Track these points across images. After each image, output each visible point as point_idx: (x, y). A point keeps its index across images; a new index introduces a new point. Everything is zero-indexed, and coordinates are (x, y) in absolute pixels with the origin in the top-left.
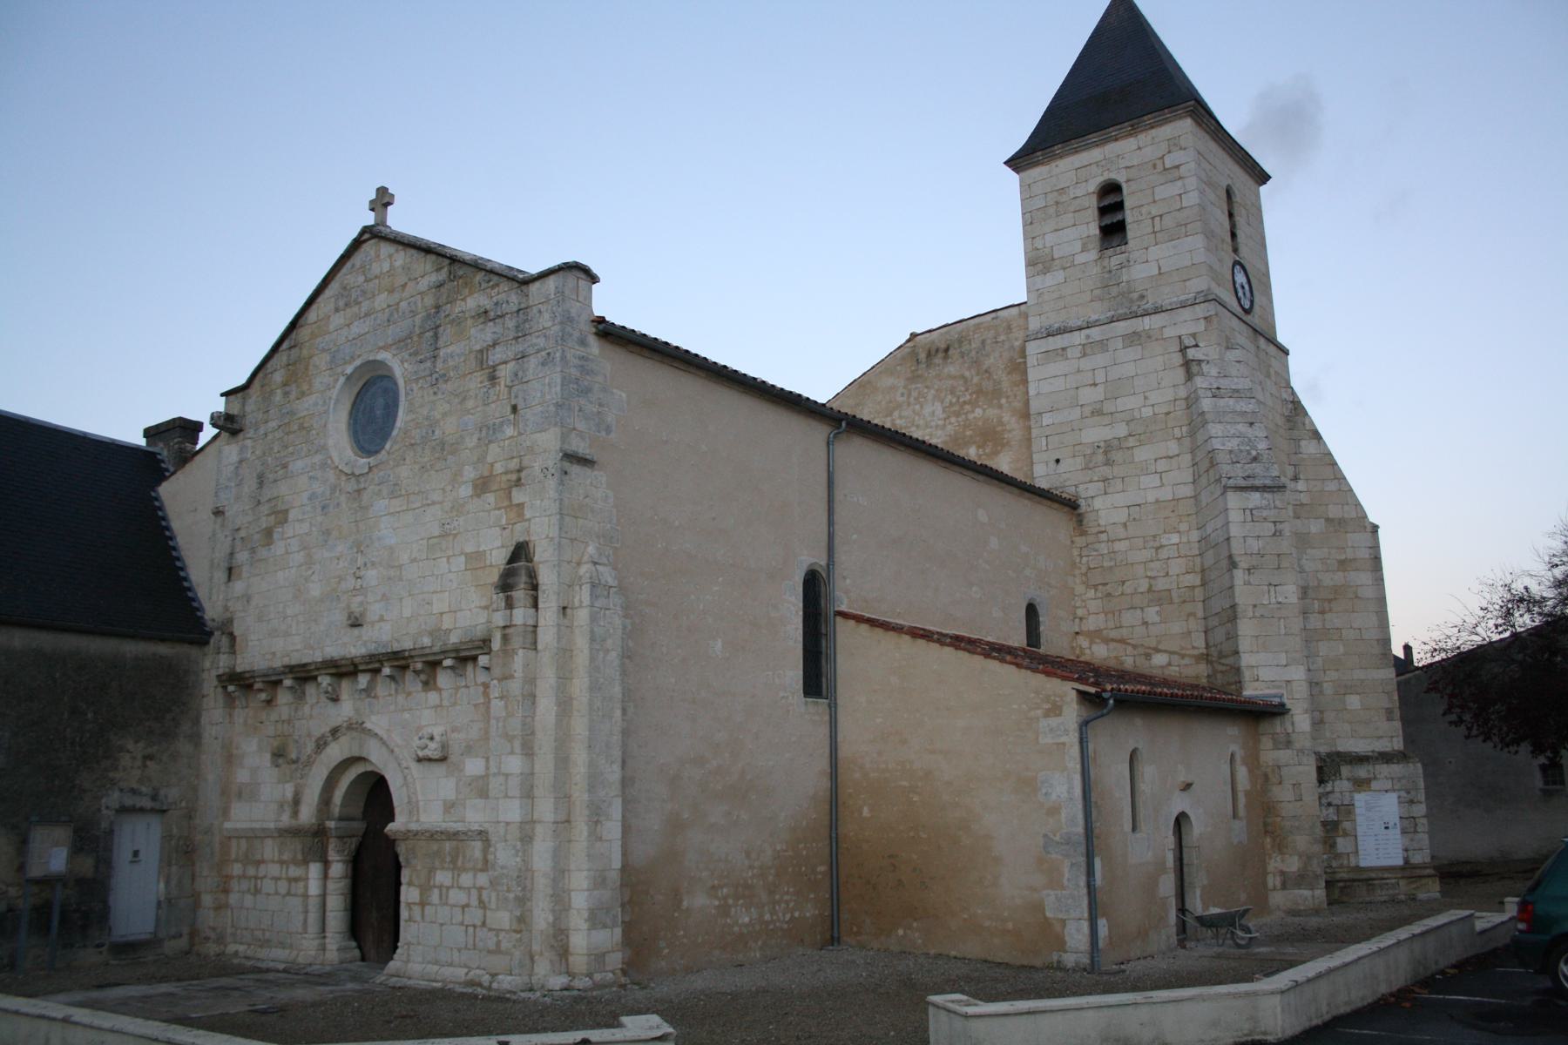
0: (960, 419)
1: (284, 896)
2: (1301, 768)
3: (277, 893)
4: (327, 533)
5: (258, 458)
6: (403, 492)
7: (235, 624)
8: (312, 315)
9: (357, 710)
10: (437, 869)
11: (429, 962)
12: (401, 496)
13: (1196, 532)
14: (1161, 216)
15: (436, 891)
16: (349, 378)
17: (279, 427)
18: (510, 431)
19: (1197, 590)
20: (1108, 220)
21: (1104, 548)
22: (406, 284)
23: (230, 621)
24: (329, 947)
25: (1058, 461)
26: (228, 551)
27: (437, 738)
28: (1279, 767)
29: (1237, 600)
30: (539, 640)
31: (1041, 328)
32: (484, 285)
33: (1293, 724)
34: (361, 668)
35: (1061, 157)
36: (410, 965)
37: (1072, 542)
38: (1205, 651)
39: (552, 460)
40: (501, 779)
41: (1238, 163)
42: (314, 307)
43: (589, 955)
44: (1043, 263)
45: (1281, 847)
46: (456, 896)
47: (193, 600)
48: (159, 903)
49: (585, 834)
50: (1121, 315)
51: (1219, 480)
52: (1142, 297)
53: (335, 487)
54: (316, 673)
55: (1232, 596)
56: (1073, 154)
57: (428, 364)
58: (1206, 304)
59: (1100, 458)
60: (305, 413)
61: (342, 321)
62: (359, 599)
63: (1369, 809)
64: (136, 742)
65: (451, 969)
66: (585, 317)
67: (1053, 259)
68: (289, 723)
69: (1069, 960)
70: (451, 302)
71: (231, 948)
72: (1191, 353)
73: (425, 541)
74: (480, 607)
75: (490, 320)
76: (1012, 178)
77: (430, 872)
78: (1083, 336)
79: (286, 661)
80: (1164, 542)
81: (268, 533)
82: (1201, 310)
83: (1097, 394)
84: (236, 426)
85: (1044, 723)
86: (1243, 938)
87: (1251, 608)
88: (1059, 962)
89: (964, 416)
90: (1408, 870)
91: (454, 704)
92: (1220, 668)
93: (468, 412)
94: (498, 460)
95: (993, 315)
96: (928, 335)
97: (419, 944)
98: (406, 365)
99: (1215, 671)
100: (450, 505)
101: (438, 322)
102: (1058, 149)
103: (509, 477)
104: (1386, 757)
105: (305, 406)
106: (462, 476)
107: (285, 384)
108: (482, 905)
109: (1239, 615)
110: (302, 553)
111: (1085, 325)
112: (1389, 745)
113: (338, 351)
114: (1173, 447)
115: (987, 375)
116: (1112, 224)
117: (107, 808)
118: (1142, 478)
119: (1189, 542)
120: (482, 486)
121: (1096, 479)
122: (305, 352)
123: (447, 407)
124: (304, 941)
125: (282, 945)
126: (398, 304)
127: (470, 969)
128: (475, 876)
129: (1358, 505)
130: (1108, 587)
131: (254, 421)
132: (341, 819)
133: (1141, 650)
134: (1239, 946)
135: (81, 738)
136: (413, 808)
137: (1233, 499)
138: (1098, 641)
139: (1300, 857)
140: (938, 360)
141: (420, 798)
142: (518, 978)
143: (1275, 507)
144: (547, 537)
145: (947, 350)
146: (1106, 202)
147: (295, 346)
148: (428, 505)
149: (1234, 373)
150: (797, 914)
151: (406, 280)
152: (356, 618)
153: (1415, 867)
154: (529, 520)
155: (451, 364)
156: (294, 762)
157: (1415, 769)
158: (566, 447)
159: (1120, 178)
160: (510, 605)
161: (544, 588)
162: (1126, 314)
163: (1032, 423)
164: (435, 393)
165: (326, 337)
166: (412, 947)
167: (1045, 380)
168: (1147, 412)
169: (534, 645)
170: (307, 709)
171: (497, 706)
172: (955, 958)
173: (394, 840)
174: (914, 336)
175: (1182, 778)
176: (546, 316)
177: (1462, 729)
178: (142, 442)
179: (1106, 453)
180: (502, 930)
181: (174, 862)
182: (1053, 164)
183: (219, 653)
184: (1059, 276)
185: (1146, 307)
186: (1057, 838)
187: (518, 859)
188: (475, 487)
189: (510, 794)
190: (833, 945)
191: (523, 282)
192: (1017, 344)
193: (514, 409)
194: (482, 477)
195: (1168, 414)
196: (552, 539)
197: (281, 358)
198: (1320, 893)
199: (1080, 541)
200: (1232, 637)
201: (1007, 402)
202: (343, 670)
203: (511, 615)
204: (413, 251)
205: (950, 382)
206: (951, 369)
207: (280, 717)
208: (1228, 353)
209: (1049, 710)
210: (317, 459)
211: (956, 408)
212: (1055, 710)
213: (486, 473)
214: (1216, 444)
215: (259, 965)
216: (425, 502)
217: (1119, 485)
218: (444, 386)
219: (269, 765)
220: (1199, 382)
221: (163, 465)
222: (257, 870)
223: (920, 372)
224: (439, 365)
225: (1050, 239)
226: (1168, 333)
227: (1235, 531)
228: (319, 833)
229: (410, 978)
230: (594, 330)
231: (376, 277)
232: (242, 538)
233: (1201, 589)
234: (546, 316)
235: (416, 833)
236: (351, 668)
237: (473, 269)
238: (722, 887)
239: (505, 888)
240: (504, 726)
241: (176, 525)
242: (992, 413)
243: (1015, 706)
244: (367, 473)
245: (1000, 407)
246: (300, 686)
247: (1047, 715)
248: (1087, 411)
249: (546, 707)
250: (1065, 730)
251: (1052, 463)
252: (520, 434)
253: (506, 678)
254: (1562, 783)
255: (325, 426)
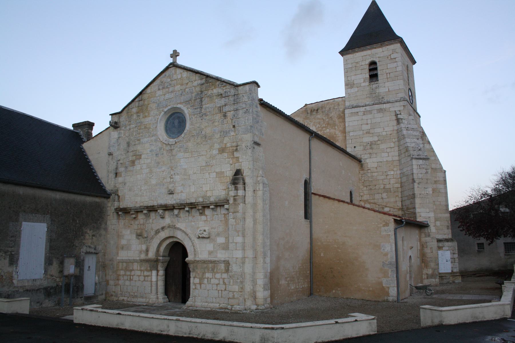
0: (322, 132)
1: (142, 282)
2: (433, 243)
3: (139, 280)
4: (158, 163)
5: (127, 137)
6: (190, 151)
7: (119, 191)
8: (148, 90)
9: (172, 222)
10: (206, 272)
11: (203, 302)
12: (189, 152)
13: (399, 171)
14: (389, 73)
15: (206, 280)
16: (165, 112)
17: (136, 127)
18: (232, 133)
19: (399, 189)
20: (372, 73)
21: (369, 175)
22: (188, 83)
23: (117, 190)
24: (159, 298)
25: (355, 147)
26: (115, 167)
27: (207, 231)
28: (426, 243)
29: (415, 192)
30: (246, 200)
31: (350, 105)
32: (220, 86)
33: (430, 230)
34: (176, 208)
35: (357, 52)
36: (196, 303)
37: (359, 172)
38: (401, 207)
39: (250, 144)
40: (234, 244)
41: (409, 58)
42: (149, 88)
43: (263, 299)
44: (351, 85)
45: (427, 266)
46: (213, 281)
47: (100, 183)
48: (96, 284)
49: (262, 261)
50: (376, 103)
51: (410, 156)
52: (383, 98)
53: (161, 148)
54: (157, 209)
55: (414, 191)
56: (361, 51)
57: (199, 110)
58: (404, 101)
59: (369, 147)
60: (147, 123)
61: (161, 93)
62: (172, 185)
63: (442, 256)
64: (90, 230)
65: (213, 304)
66: (257, 99)
67: (354, 84)
68: (143, 225)
69: (390, 299)
70: (207, 90)
71: (121, 298)
72: (399, 116)
73: (199, 167)
74: (222, 189)
75: (223, 97)
76: (341, 58)
77: (203, 273)
78: (364, 109)
79: (142, 204)
80: (389, 174)
81: (133, 163)
82: (402, 103)
83: (368, 127)
84: (118, 126)
85: (383, 228)
86: (429, 293)
87: (419, 195)
88: (387, 300)
89: (323, 131)
90: (452, 274)
91: (212, 220)
92: (407, 212)
93: (216, 126)
94: (228, 142)
95: (333, 100)
96: (311, 105)
97: (199, 296)
98: (189, 109)
99: (405, 214)
100: (209, 156)
101: (202, 97)
102: (356, 50)
103: (233, 148)
104: (447, 240)
105: (147, 121)
106: (214, 147)
107: (137, 113)
108: (224, 283)
109: (416, 197)
110: (148, 169)
111: (365, 105)
112: (448, 236)
113: (160, 103)
114: (392, 145)
115: (331, 119)
116: (373, 74)
117: (83, 252)
118: (382, 154)
119: (397, 174)
120: (222, 150)
121: (367, 153)
122: (146, 103)
123: (207, 124)
124: (151, 296)
125: (142, 297)
126: (185, 89)
127: (220, 304)
128: (221, 275)
129: (440, 164)
130: (371, 186)
131: (124, 124)
132: (163, 256)
133: (381, 206)
134: (428, 295)
135: (75, 229)
136: (195, 253)
137: (414, 162)
138: (367, 203)
139: (432, 269)
140: (314, 113)
141: (198, 250)
142: (242, 306)
143: (426, 165)
144: (248, 168)
145: (317, 110)
146: (371, 67)
147: (141, 100)
148: (200, 156)
149: (412, 123)
150: (303, 286)
151: (188, 82)
152: (172, 191)
153: (455, 273)
154: (241, 162)
155: (208, 110)
156: (146, 238)
157: (455, 244)
158: (254, 140)
159: (377, 60)
160: (236, 189)
161: (248, 184)
162: (378, 103)
163: (347, 134)
164: (202, 119)
165: (155, 98)
166: (196, 297)
167: (351, 122)
168: (384, 133)
169: (244, 202)
170: (151, 221)
171: (231, 221)
172: (353, 299)
173: (188, 263)
174: (306, 105)
175: (410, 245)
176: (246, 97)
177: (464, 232)
178: (72, 128)
179: (370, 145)
180: (235, 292)
181: (100, 270)
182: (355, 54)
183: (114, 201)
184: (356, 89)
185: (384, 101)
186: (387, 263)
187: (241, 269)
188: (219, 150)
189: (237, 249)
190: (311, 295)
191: (238, 86)
192: (341, 110)
193: (234, 126)
194: (222, 148)
195: (391, 134)
196: (250, 169)
197: (136, 103)
198: (437, 280)
199: (361, 172)
200: (413, 203)
201: (338, 128)
202: (168, 208)
203: (237, 192)
204: (190, 72)
205: (318, 120)
206: (319, 116)
207: (139, 222)
208: (410, 117)
209: (384, 224)
210: (153, 138)
211: (320, 129)
212: (387, 224)
213: (224, 146)
214: (409, 145)
215: (135, 303)
216: (199, 155)
217: (375, 156)
218: (205, 117)
219: (135, 238)
220: (402, 125)
221: (82, 137)
222: (131, 273)
223: (308, 117)
224: (203, 111)
225: (353, 78)
226: (392, 109)
227: (415, 171)
228: (157, 261)
229: (197, 307)
230: (259, 103)
231: (175, 80)
232: (121, 163)
233: (400, 188)
234: (246, 97)
235: (198, 261)
236: (172, 208)
237: (216, 80)
238: (288, 277)
239: (236, 278)
240: (235, 227)
241: (91, 157)
242: (332, 131)
243: (373, 223)
244: (175, 144)
245: (335, 129)
246: (149, 213)
247: (384, 226)
248: (365, 132)
249: (249, 222)
250: (390, 231)
251: (353, 148)
252: (236, 135)
253: (236, 212)
254: (483, 248)
255: (156, 127)
